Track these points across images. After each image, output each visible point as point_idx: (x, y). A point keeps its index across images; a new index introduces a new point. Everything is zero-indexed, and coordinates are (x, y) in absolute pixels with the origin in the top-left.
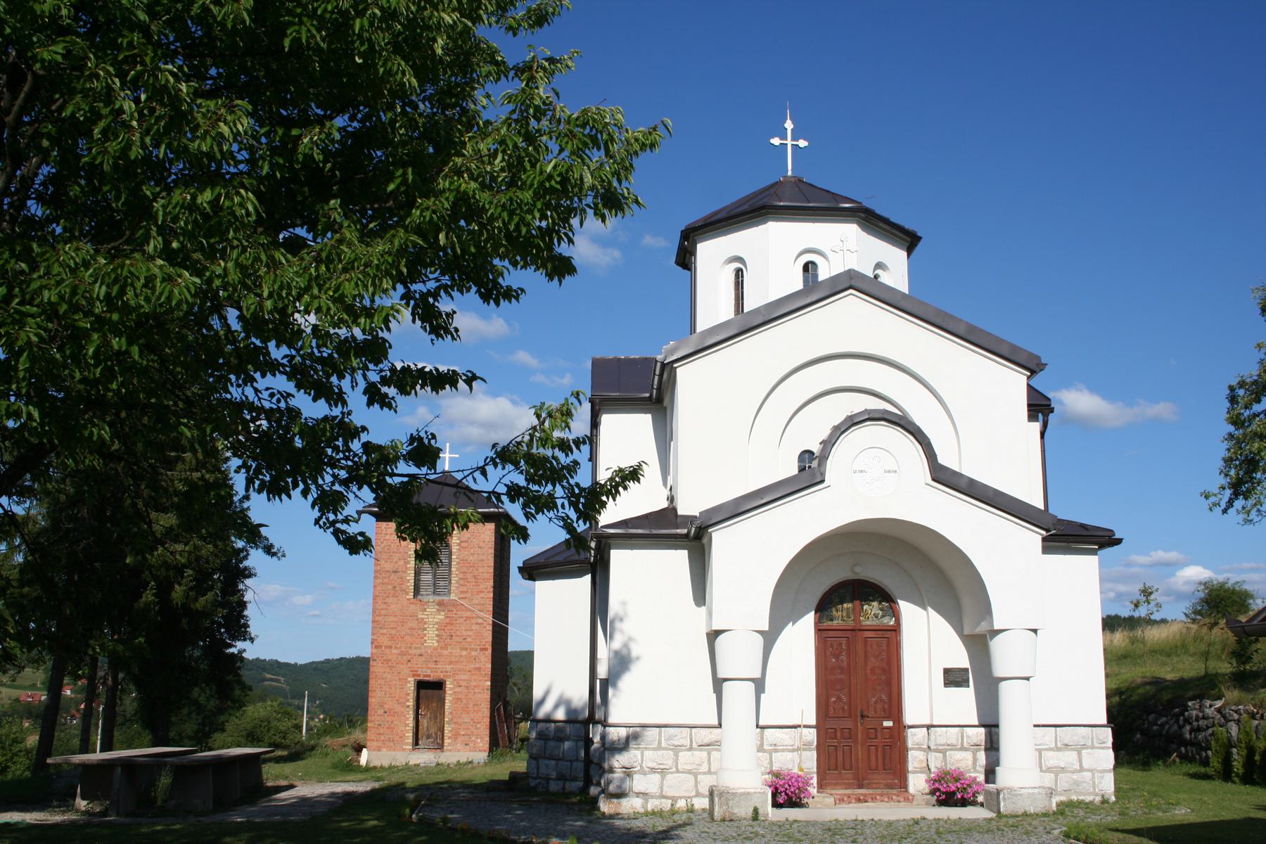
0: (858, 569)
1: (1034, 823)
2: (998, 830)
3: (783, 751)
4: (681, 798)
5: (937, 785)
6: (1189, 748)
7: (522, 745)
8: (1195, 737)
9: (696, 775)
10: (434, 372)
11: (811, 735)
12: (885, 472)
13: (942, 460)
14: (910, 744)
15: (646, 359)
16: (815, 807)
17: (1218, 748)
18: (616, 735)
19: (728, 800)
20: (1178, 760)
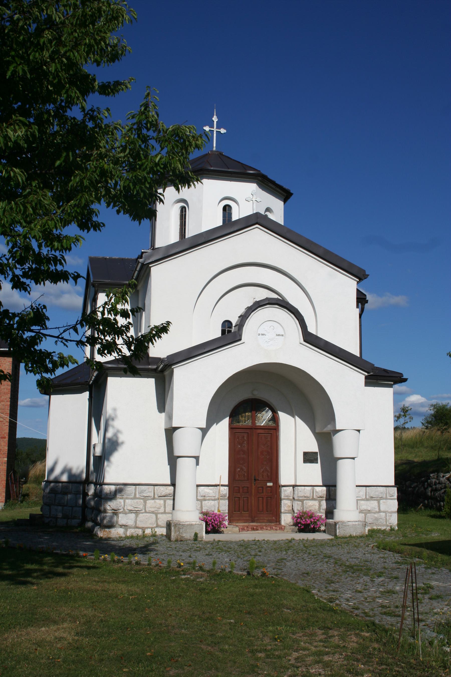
0: (256, 393)
1: (357, 541)
2: (339, 545)
3: (209, 500)
4: (147, 528)
5: (299, 520)
6: (430, 501)
7: (24, 498)
8: (434, 494)
9: (156, 514)
10: (54, 271)
11: (225, 490)
12: (277, 335)
13: (311, 329)
14: (283, 497)
15: (122, 259)
16: (228, 533)
17: (449, 500)
18: (109, 490)
19: (179, 528)
20: (423, 508)
